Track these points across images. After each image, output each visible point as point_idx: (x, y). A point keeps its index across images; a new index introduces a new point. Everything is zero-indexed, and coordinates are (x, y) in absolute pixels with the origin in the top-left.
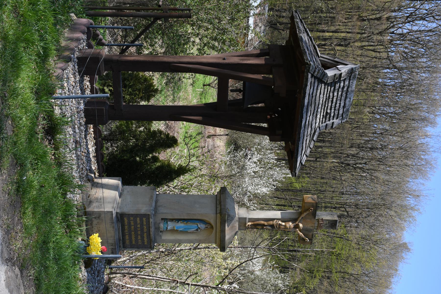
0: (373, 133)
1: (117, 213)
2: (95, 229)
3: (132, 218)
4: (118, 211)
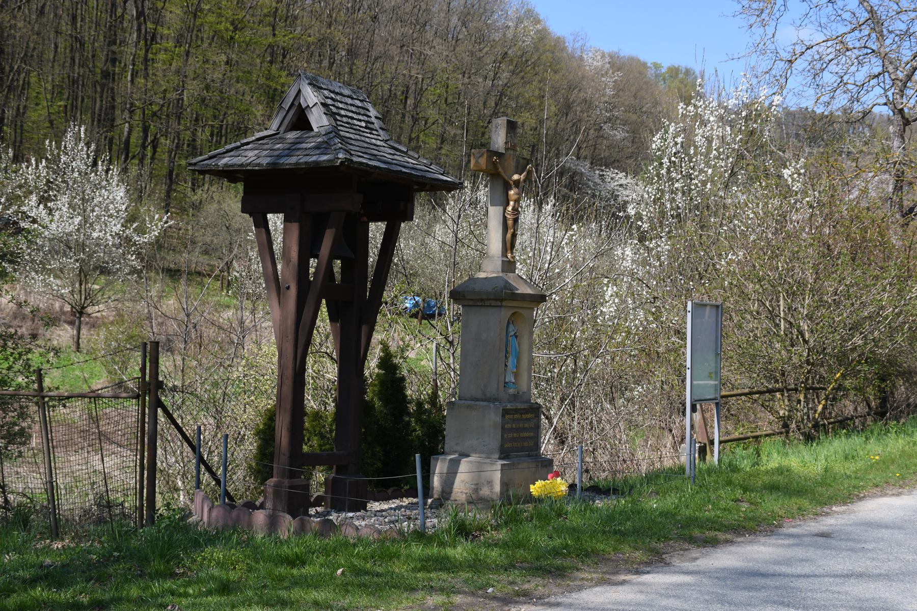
1: (500, 458)
2: (521, 491)
4: (497, 456)
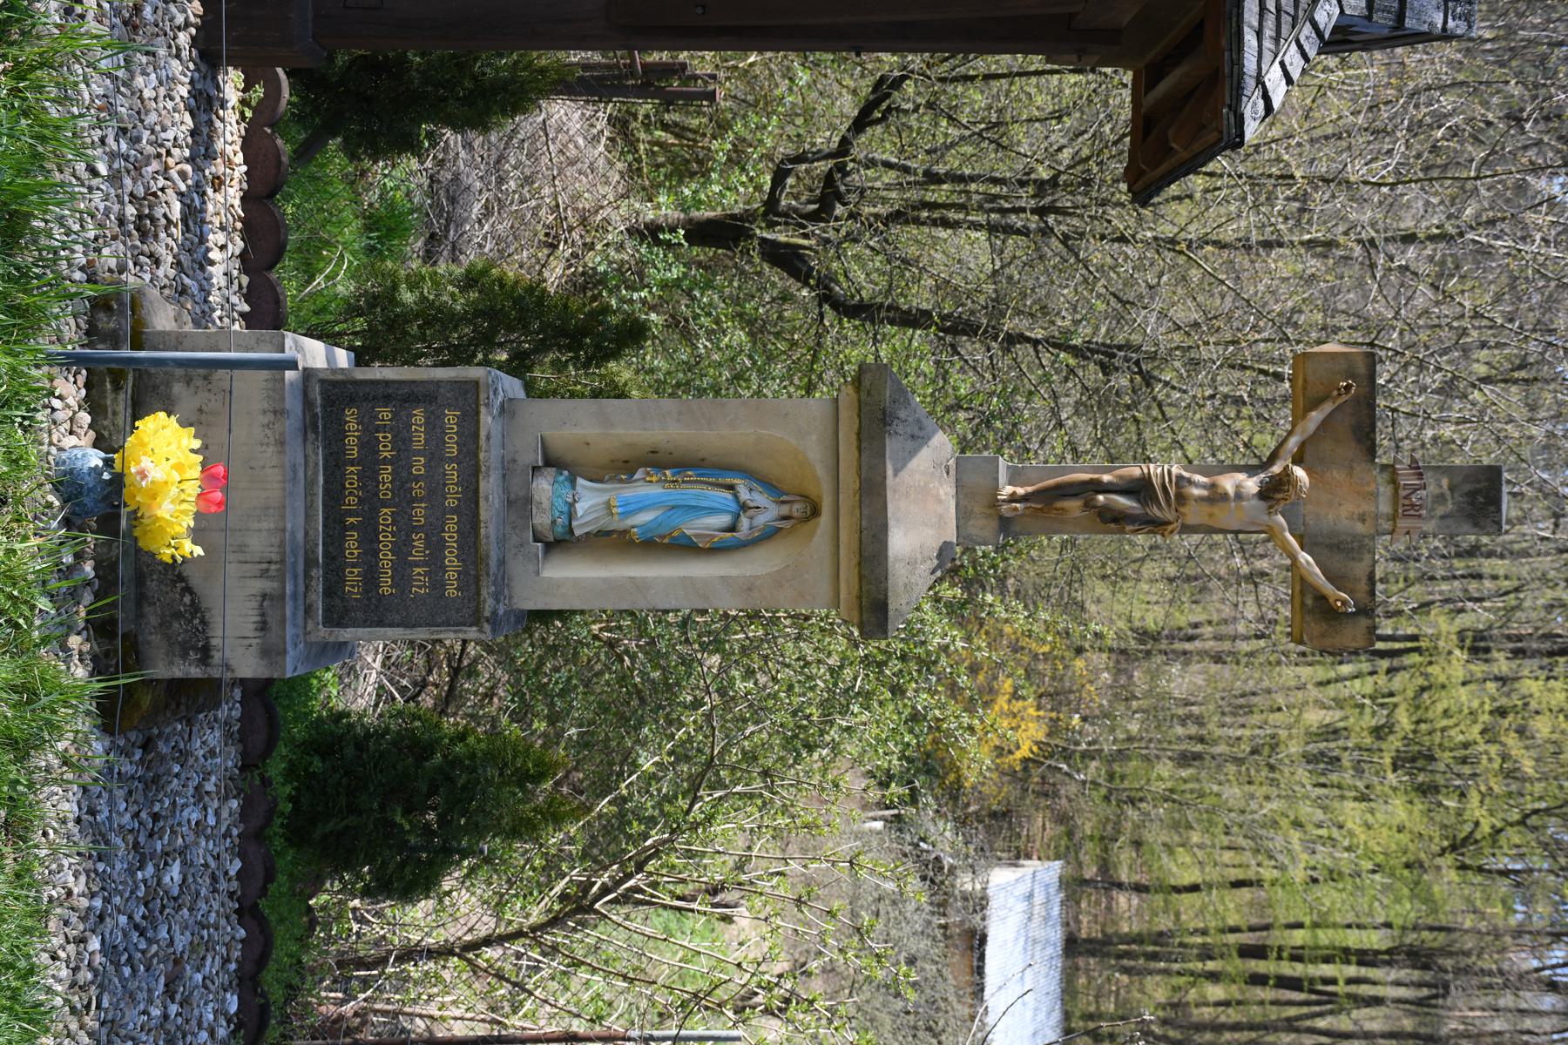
0: (1246, 952)
3: (385, 413)
